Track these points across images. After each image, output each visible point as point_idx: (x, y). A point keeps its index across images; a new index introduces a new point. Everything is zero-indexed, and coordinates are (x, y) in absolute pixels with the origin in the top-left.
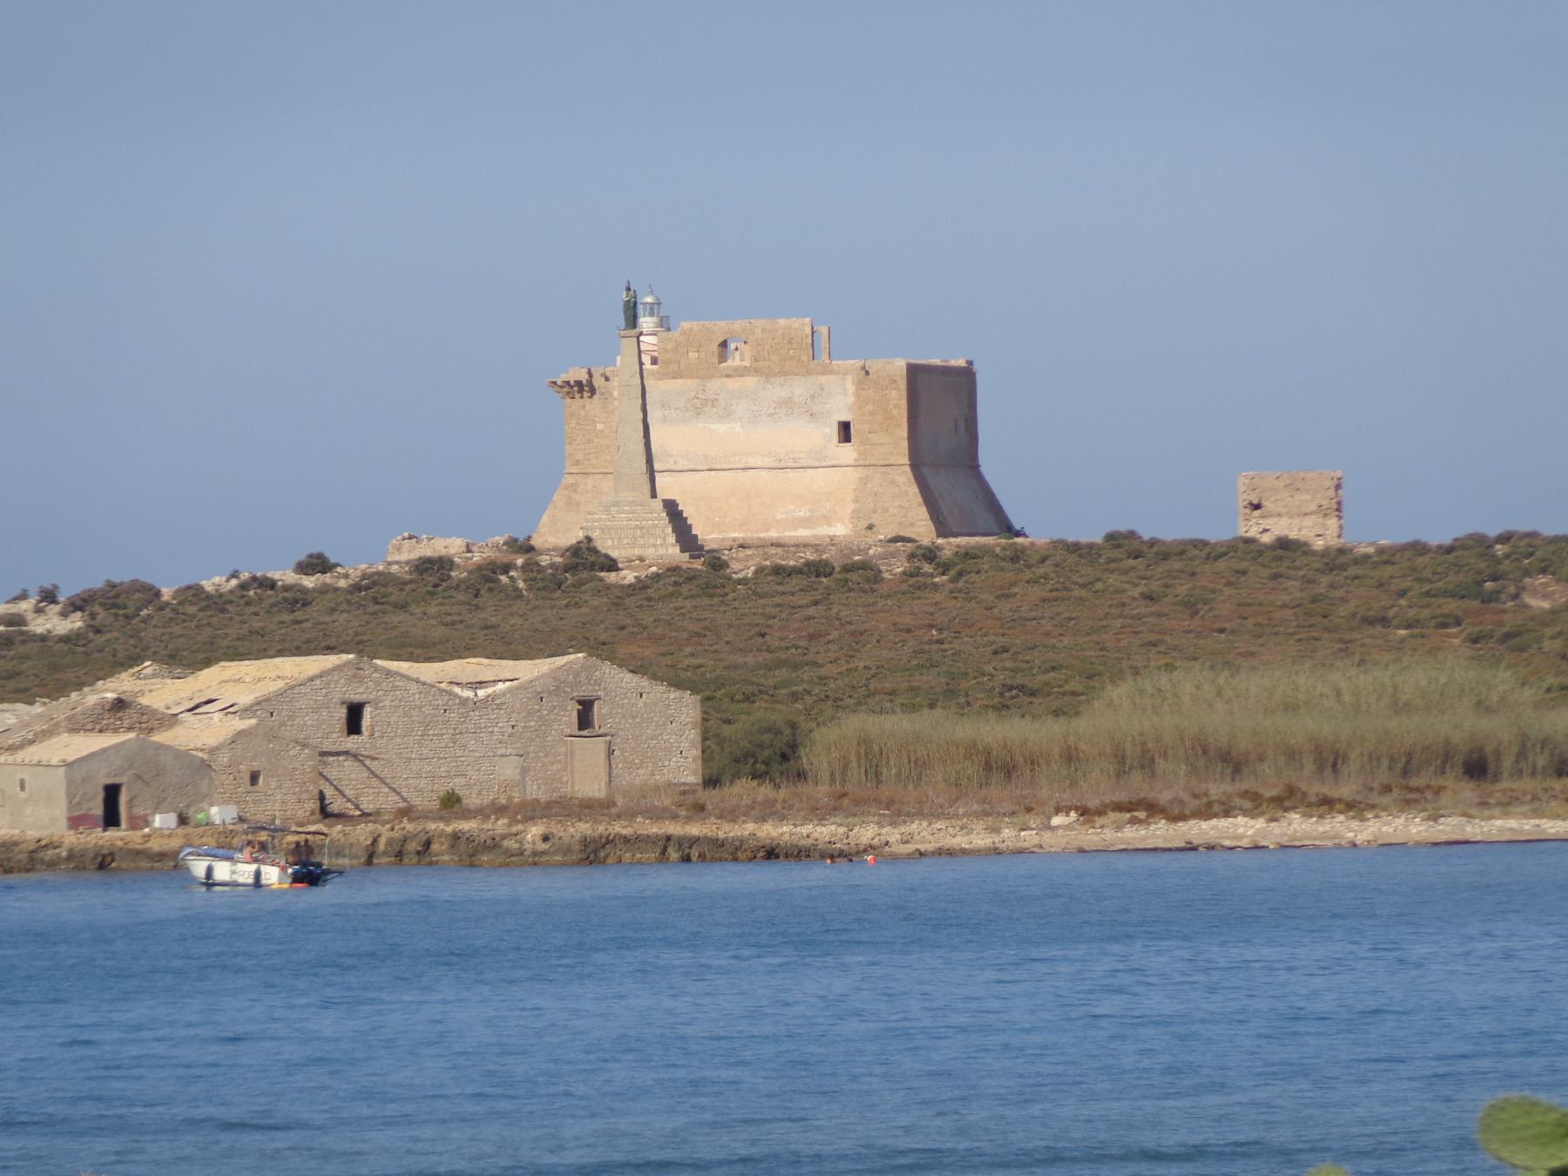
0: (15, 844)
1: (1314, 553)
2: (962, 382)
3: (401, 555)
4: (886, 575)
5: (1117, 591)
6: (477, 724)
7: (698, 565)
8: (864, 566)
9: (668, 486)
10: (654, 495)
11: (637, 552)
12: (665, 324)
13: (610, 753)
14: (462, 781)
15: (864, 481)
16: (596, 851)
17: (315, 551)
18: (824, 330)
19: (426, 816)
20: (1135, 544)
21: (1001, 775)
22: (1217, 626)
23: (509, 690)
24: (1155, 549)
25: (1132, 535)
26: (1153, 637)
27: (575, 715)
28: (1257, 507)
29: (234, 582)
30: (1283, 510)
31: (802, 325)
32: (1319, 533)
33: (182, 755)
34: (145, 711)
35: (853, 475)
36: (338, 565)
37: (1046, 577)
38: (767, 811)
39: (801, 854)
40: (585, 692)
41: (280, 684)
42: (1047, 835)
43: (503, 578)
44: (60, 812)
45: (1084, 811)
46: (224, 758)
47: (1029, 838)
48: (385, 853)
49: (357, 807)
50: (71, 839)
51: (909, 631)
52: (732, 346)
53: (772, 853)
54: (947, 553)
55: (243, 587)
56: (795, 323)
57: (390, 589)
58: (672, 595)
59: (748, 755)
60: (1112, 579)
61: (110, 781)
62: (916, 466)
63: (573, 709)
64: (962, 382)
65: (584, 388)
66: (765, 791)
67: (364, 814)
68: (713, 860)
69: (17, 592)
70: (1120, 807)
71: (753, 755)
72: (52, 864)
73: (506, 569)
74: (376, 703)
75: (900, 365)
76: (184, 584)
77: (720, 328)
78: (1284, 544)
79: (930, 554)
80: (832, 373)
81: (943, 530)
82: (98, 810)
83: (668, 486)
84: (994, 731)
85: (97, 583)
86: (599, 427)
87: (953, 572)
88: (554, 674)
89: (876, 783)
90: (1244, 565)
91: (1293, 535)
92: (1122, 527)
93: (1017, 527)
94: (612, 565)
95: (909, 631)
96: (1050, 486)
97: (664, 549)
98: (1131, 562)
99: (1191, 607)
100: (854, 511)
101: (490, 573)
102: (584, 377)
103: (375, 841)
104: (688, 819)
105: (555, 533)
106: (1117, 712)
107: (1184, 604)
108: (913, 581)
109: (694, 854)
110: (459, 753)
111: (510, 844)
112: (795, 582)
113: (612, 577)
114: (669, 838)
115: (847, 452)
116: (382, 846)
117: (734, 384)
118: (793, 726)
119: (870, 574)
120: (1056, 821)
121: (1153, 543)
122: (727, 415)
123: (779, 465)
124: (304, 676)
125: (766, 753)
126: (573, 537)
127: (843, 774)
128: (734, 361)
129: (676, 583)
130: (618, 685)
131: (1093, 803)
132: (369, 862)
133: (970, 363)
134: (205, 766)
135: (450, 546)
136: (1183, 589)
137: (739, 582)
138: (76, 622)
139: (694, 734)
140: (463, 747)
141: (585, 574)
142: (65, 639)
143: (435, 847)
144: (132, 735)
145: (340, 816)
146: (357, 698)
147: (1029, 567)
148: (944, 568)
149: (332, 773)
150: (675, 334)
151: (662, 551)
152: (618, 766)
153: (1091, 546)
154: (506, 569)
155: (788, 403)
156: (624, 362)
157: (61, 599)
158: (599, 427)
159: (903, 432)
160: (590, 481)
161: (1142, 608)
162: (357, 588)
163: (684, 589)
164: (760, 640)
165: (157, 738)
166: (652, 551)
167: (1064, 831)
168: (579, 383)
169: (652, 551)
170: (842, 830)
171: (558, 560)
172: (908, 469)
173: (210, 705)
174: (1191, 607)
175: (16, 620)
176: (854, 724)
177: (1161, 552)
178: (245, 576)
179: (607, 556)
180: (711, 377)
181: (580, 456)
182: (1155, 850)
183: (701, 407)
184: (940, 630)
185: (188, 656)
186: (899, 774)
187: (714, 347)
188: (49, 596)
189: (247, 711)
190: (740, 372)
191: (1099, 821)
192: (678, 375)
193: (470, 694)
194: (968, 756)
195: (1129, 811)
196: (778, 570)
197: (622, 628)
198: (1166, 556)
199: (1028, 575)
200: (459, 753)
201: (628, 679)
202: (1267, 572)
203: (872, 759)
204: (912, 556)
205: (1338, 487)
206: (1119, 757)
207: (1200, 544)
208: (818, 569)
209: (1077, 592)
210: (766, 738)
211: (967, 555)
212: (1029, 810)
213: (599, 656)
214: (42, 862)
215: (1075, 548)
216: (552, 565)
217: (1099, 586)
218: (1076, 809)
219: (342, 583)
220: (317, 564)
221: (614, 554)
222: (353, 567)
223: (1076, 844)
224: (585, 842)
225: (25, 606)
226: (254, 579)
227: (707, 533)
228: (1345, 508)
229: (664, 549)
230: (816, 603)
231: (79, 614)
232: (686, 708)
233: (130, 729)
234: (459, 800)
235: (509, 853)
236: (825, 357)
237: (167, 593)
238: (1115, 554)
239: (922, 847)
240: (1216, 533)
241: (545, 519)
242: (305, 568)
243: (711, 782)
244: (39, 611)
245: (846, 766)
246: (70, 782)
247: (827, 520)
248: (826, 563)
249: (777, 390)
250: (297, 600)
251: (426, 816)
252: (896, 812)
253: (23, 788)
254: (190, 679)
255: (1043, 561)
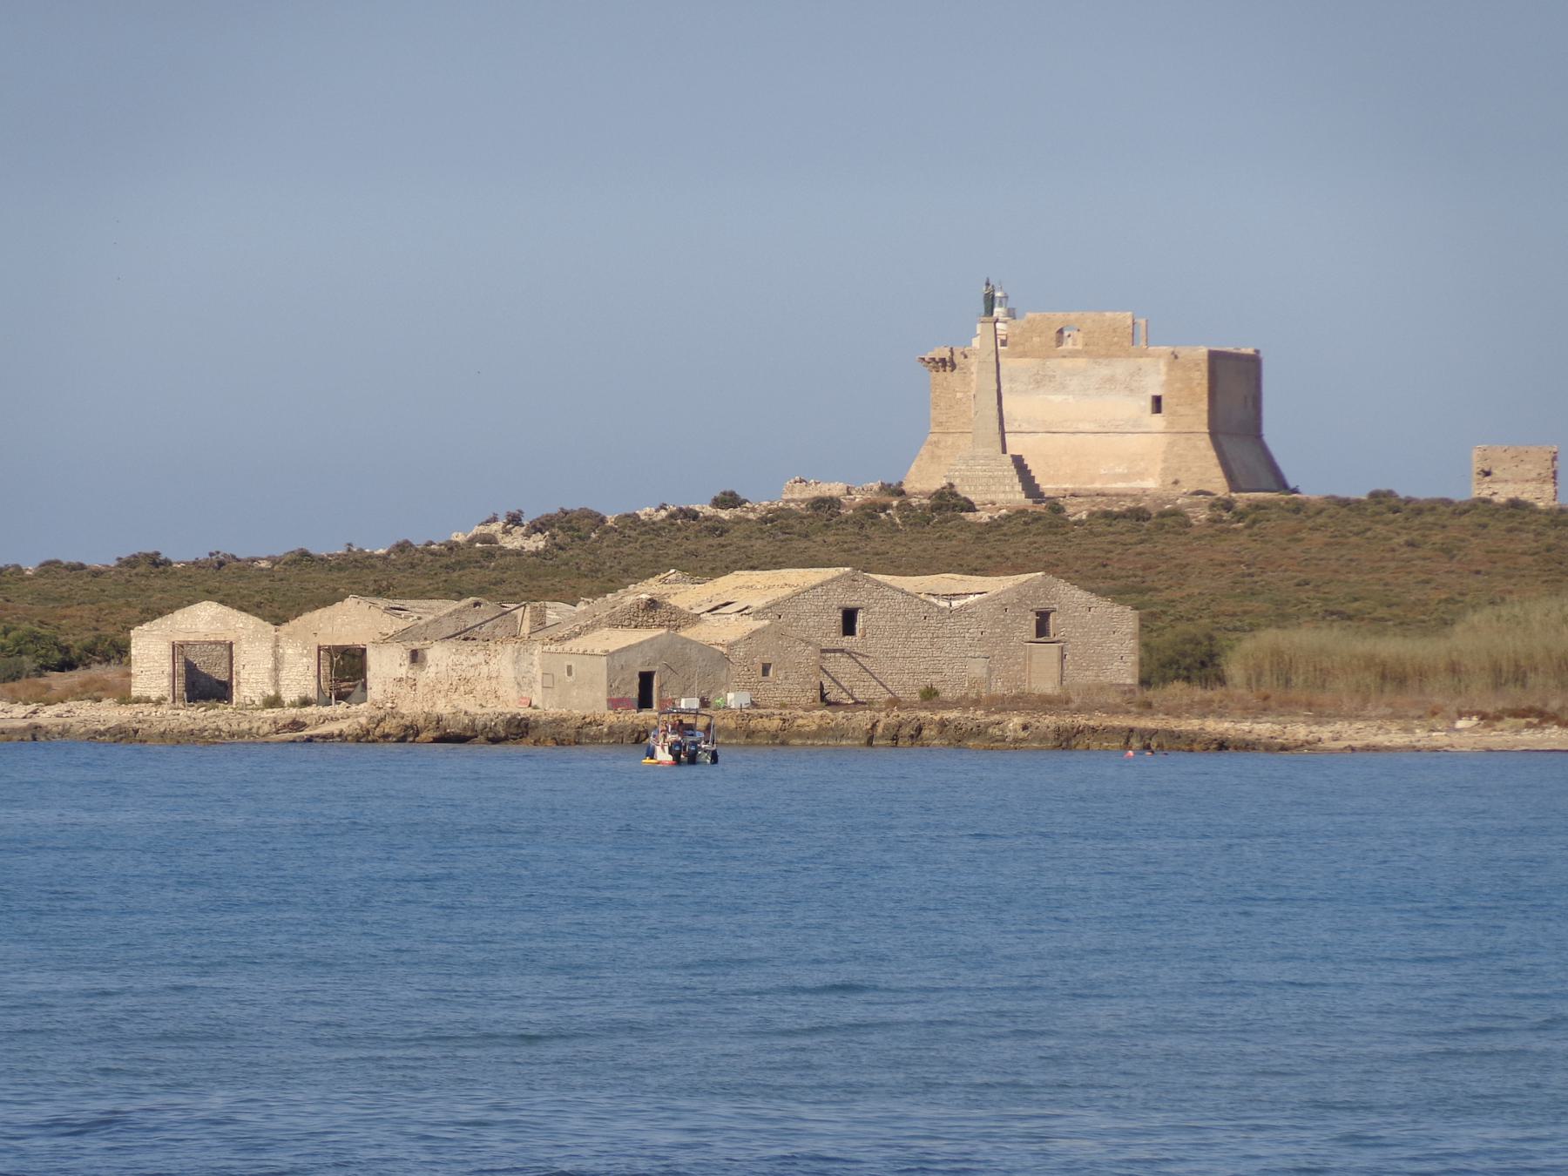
0: (564, 720)
1: (1540, 512)
2: (1250, 367)
3: (796, 494)
4: (1193, 521)
5: (1385, 539)
6: (951, 629)
7: (1041, 508)
8: (1175, 513)
9: (1015, 445)
10: (1004, 451)
11: (989, 497)
12: (1011, 314)
13: (1063, 657)
14: (938, 677)
15: (1171, 445)
16: (1068, 740)
17: (728, 489)
18: (1142, 322)
19: (911, 706)
20: (1393, 501)
21: (1394, 683)
22: (1474, 568)
23: (979, 602)
24: (1411, 506)
25: (1390, 494)
26: (1424, 577)
27: (1034, 623)
28: (1488, 474)
29: (663, 513)
30: (1509, 477)
31: (1127, 317)
32: (1541, 496)
33: (704, 648)
34: (674, 610)
35: (1163, 440)
36: (745, 501)
37: (1325, 525)
38: (1206, 710)
39: (1247, 746)
40: (1042, 605)
41: (788, 591)
42: (1455, 737)
43: (882, 515)
44: (602, 695)
45: (1483, 716)
46: (740, 652)
47: (1440, 738)
48: (882, 737)
49: (851, 696)
50: (611, 718)
51: (1223, 565)
52: (1066, 333)
53: (1222, 745)
54: (1240, 505)
55: (672, 516)
56: (1119, 315)
57: (791, 522)
58: (1023, 532)
59: (1172, 662)
60: (1379, 528)
61: (645, 669)
62: (1213, 434)
63: (1032, 620)
64: (1250, 367)
65: (946, 364)
66: (1199, 693)
67: (857, 703)
68: (1170, 749)
69: (490, 515)
70: (1516, 714)
71: (1177, 662)
72: (595, 739)
73: (884, 508)
74: (868, 610)
75: (1203, 351)
76: (623, 513)
77: (1058, 318)
78: (1515, 504)
79: (1228, 505)
80: (1148, 356)
81: (1234, 486)
82: (634, 694)
83: (1015, 445)
84: (1391, 647)
85: (553, 510)
86: (959, 395)
87: (1247, 521)
88: (1017, 589)
89: (1283, 687)
90: (1484, 520)
91: (1525, 497)
92: (1383, 487)
93: (1292, 485)
94: (970, 507)
95: (1223, 565)
96: (1325, 448)
97: (1012, 495)
98: (1391, 516)
99: (1447, 551)
100: (457, 544)
101: (870, 512)
102: (947, 355)
103: (874, 725)
104: (1140, 715)
105: (922, 480)
106: (1478, 635)
107: (1442, 550)
108: (1219, 526)
109: (1154, 745)
110: (936, 654)
111: (995, 731)
112: (1121, 525)
113: (970, 516)
114: (1132, 730)
115: (1158, 421)
116: (880, 730)
117: (1068, 363)
118: (1211, 638)
119: (1181, 519)
120: (1460, 724)
121: (1408, 501)
122: (1063, 388)
123: (1110, 432)
124: (808, 585)
125: (1188, 661)
126: (938, 483)
127: (1258, 681)
128: (1068, 345)
129: (1026, 523)
130: (1070, 598)
131: (1490, 710)
132: (869, 743)
133: (1257, 351)
134: (724, 659)
135: (834, 489)
136: (1437, 537)
137: (1075, 523)
138: (538, 542)
139: (1133, 644)
140: (941, 649)
141: (949, 514)
142: (537, 554)
143: (925, 733)
144: (663, 631)
145: (836, 705)
146: (851, 604)
147: (1309, 517)
148: (1240, 516)
149: (828, 666)
150: (1020, 322)
151: (1010, 496)
152: (1069, 668)
153: (1359, 501)
154: (884, 508)
155: (1111, 379)
156: (980, 341)
157: (525, 522)
158: (959, 395)
159: (1204, 406)
160: (950, 440)
161: (1407, 553)
162: (764, 520)
163: (1034, 527)
164: (1103, 570)
165: (683, 633)
166: (1002, 496)
167: (1466, 734)
168: (943, 360)
169: (1002, 496)
170: (1277, 727)
171: (926, 501)
172: (1207, 437)
173: (729, 608)
174: (1447, 551)
175: (489, 539)
176: (1269, 637)
177: (1417, 509)
178: (672, 508)
179: (966, 499)
180: (1048, 357)
181: (944, 419)
182: (518, 730)
183: (1040, 381)
184: (1248, 566)
185: (704, 568)
186: (1306, 681)
187: (1053, 333)
188: (515, 520)
189: (760, 613)
190: (1074, 354)
191: (1499, 725)
192: (1023, 355)
193: (946, 604)
194: (1367, 667)
195: (1524, 717)
196: (1107, 515)
197: (989, 557)
198: (1419, 512)
199: (1309, 524)
200: (936, 654)
201: (1079, 595)
202: (1504, 526)
203: (1283, 667)
204: (1212, 506)
205: (1554, 459)
206: (1496, 671)
207: (1447, 502)
208: (1139, 515)
209: (1354, 539)
210: (1188, 647)
211: (1257, 506)
212: (1434, 714)
213: (1054, 574)
214: (587, 735)
215: (1345, 503)
216: (921, 506)
217: (1369, 534)
218: (1477, 713)
219: (751, 516)
220: (729, 500)
221: (972, 498)
222: (760, 502)
223: (1483, 744)
224: (1058, 731)
225: (495, 528)
226: (681, 510)
227: (1047, 486)
228: (1560, 476)
229: (1012, 495)
230: (1142, 542)
231: (539, 536)
232: (1126, 620)
233: (660, 626)
234: (937, 693)
235: (994, 739)
236: (1142, 343)
237: (610, 520)
238: (1378, 508)
239: (1354, 743)
240: (1458, 495)
241: (913, 469)
242: (719, 503)
243: (1145, 682)
244: (507, 532)
245: (1260, 675)
246: (610, 669)
247: (1141, 476)
248: (1143, 510)
249: (1103, 370)
250: (717, 529)
251: (911, 706)
252: (1320, 715)
253: (570, 673)
254: (709, 584)
255: (1319, 512)
